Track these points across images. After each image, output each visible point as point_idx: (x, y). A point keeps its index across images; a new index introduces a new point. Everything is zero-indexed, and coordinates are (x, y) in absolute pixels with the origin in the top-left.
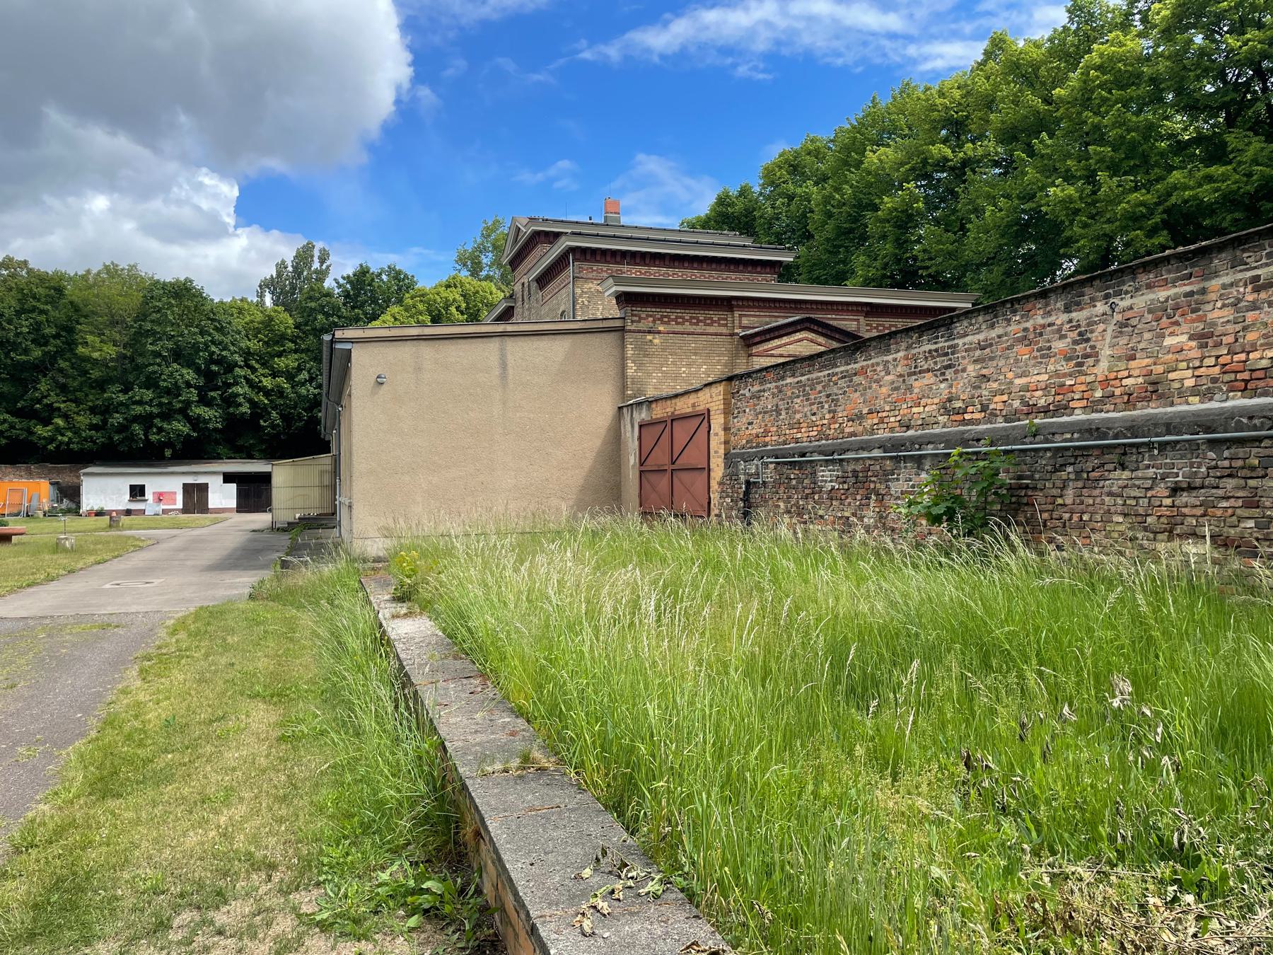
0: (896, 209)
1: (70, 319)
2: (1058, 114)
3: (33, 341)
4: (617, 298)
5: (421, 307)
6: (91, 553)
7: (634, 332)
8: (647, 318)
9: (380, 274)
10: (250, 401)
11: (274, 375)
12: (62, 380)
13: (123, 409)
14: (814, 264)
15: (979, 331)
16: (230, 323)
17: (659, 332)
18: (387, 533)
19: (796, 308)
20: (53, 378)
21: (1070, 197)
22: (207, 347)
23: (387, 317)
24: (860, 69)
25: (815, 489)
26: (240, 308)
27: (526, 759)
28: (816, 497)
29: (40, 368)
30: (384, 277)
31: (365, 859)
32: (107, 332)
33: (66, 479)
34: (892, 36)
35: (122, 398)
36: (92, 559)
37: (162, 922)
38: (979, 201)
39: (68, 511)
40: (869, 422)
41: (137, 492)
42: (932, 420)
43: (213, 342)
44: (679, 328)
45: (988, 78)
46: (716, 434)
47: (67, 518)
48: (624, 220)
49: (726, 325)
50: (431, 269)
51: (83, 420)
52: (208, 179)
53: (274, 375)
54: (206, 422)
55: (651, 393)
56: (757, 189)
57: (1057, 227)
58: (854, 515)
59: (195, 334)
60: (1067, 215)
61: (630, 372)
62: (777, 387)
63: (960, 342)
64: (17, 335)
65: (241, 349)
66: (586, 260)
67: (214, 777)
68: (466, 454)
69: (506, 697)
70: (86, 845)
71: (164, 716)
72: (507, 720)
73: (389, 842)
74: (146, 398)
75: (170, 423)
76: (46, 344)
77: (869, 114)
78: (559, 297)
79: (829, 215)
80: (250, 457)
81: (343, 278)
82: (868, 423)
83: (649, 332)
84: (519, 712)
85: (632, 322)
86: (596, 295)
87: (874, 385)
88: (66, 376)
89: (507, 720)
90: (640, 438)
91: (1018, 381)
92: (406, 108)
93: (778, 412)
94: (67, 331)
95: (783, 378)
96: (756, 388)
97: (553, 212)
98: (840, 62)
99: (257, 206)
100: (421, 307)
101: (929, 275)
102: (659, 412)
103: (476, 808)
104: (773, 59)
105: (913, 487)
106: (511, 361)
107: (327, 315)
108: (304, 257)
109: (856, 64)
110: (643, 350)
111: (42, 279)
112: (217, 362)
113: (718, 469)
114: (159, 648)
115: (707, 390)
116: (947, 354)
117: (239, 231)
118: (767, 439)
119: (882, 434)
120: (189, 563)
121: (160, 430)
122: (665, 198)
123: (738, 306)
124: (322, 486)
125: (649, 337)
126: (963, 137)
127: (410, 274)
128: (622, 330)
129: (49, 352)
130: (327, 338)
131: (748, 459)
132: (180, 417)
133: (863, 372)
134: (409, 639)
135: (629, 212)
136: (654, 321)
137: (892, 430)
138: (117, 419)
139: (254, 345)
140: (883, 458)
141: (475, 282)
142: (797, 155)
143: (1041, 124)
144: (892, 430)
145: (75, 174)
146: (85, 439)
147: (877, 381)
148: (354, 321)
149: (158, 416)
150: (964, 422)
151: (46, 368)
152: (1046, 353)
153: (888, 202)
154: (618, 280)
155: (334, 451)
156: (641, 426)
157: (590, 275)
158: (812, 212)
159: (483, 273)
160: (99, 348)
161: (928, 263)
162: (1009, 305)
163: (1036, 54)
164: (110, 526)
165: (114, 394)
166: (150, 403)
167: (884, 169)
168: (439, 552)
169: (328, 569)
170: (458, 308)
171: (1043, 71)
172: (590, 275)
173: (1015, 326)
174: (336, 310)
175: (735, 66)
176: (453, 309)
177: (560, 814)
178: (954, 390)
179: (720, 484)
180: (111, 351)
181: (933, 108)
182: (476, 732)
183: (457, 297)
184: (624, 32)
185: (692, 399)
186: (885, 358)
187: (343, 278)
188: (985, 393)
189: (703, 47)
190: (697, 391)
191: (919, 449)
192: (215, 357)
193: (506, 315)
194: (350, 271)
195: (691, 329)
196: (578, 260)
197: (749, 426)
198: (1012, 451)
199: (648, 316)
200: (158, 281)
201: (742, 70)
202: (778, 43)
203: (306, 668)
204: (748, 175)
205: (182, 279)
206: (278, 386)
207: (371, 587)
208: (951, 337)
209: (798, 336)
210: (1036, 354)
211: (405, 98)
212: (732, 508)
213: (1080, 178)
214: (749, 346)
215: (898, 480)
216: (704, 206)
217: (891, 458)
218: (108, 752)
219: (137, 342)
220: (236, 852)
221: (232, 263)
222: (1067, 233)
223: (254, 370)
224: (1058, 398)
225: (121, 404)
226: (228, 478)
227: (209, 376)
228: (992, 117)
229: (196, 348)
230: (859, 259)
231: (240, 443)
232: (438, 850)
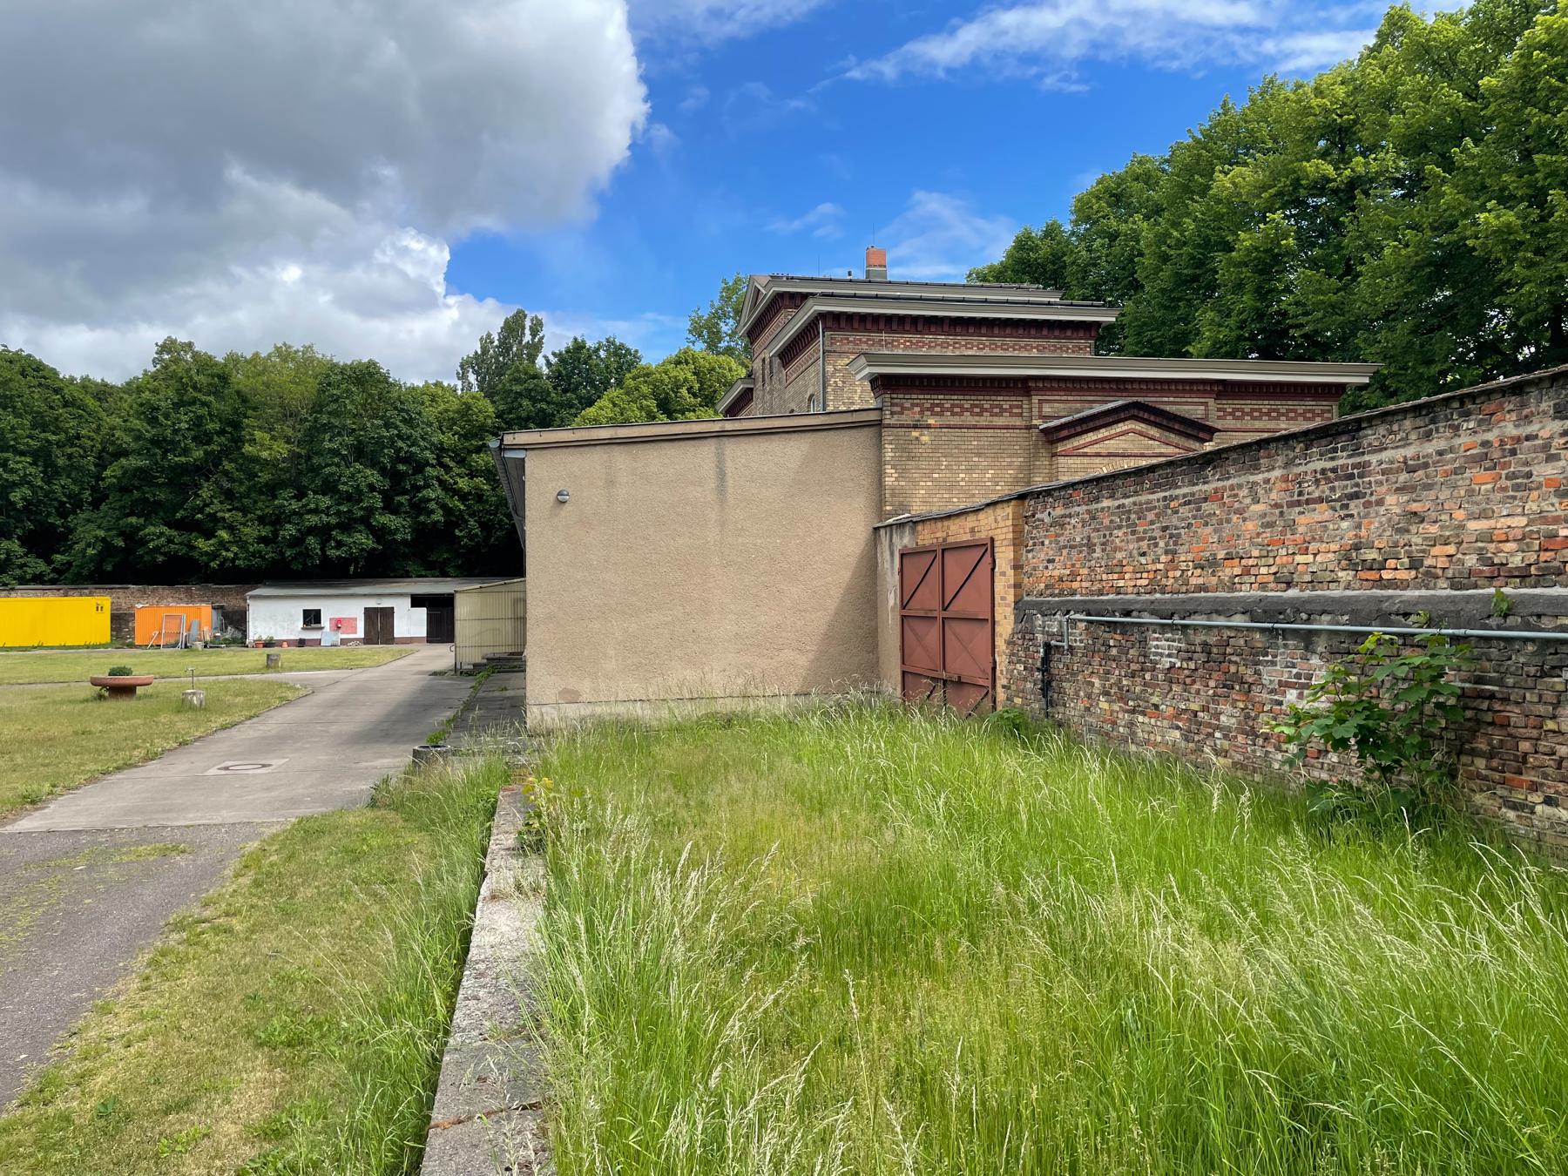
0: (1256, 249)
1: (235, 411)
2: (1488, 112)
3: (194, 439)
4: (872, 382)
5: (645, 389)
8: (912, 407)
9: (597, 350)
10: (444, 507)
11: (472, 475)
13: (295, 519)
14: (1145, 324)
15: (1405, 442)
16: (419, 414)
17: (929, 427)
19: (1119, 390)
21: (1508, 225)
24: (1201, 74)
25: (1146, 664)
26: (434, 394)
28: (1148, 676)
29: (202, 470)
30: (602, 354)
33: (231, 602)
34: (1243, 30)
35: (295, 505)
36: (221, 720)
38: (1372, 234)
40: (1228, 571)
41: (312, 618)
42: (1328, 576)
43: (400, 436)
44: (956, 421)
45: (1384, 68)
46: (1003, 574)
48: (894, 274)
49: (1021, 415)
50: (656, 340)
51: (250, 532)
52: (415, 244)
53: (472, 475)
55: (918, 509)
56: (1068, 227)
57: (1487, 265)
58: (1205, 709)
59: (378, 427)
60: (1505, 250)
61: (889, 481)
62: (1089, 512)
63: (1373, 459)
64: (176, 432)
66: (840, 329)
68: (686, 581)
74: (323, 506)
75: (350, 536)
76: (208, 443)
77: (1219, 123)
78: (807, 375)
79: (1165, 258)
80: (445, 574)
82: (1226, 572)
83: (915, 427)
85: (892, 413)
87: (1235, 518)
88: (232, 480)
90: (901, 571)
91: (1473, 525)
93: (1091, 547)
94: (233, 426)
95: (1097, 500)
96: (1059, 511)
97: (802, 268)
98: (1175, 65)
99: (471, 270)
100: (645, 389)
101: (1305, 336)
102: (928, 537)
104: (1089, 66)
105: (1302, 687)
106: (730, 466)
107: (534, 401)
108: (513, 328)
109: (1196, 67)
111: (204, 363)
112: (404, 461)
113: (1006, 624)
115: (990, 511)
116: (1351, 477)
117: (451, 300)
118: (1075, 585)
119: (1247, 592)
121: (339, 544)
122: (946, 245)
123: (1038, 389)
125: (915, 434)
126: (1349, 149)
127: (633, 348)
128: (878, 424)
129: (212, 451)
131: (1048, 611)
132: (362, 528)
133: (1216, 496)
135: (899, 262)
136: (922, 412)
137: (1263, 586)
138: (289, 530)
139: (448, 439)
140: (1248, 629)
141: (711, 357)
142: (1121, 180)
143: (1463, 127)
144: (1263, 586)
145: (266, 237)
146: (253, 554)
147: (1240, 512)
149: (338, 526)
150: (1380, 583)
151: (210, 472)
152: (1523, 483)
153: (1246, 240)
154: (872, 359)
156: (902, 556)
157: (845, 348)
158: (1141, 254)
159: (723, 345)
160: (269, 446)
161: (1303, 320)
162: (1456, 405)
163: (1452, 32)
164: (268, 666)
167: (1239, 195)
170: (689, 390)
171: (1462, 56)
173: (1468, 437)
174: (544, 396)
175: (1040, 77)
176: (684, 391)
178: (1363, 532)
180: (282, 449)
181: (1307, 111)
185: (970, 521)
186: (1252, 478)
188: (1415, 540)
189: (998, 56)
190: (977, 511)
191: (1308, 621)
192: (402, 454)
194: (562, 347)
195: (972, 420)
196: (830, 329)
197: (1050, 564)
198: (1466, 637)
200: (336, 365)
201: (1050, 82)
202: (1095, 46)
204: (1056, 207)
208: (1357, 451)
209: (1121, 427)
210: (1504, 483)
212: (1025, 679)
213: (1522, 199)
214: (1053, 442)
215: (1273, 663)
216: (998, 253)
217: (1263, 630)
221: (424, 335)
222: (1504, 276)
223: (448, 469)
224: (1545, 556)
225: (294, 513)
226: (417, 601)
227: (395, 477)
228: (1392, 119)
230: (1205, 316)
231: (433, 558)
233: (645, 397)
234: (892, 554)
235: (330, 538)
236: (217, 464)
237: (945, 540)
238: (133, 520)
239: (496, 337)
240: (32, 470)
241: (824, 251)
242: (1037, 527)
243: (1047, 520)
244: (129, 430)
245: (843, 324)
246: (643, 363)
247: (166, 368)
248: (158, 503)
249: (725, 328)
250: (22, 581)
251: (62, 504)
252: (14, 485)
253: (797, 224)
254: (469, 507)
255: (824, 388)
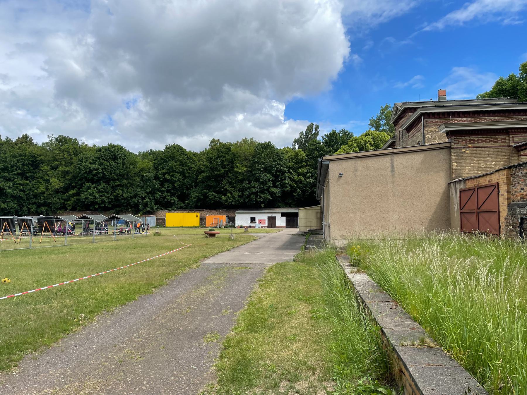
5: (355, 145)
6: (240, 241)
7: (456, 148)
8: (462, 141)
10: (290, 185)
12: (230, 180)
17: (469, 147)
18: (343, 237)
20: (227, 180)
22: (276, 166)
23: (341, 150)
26: (286, 151)
27: (422, 341)
29: (224, 176)
31: (351, 373)
32: (243, 163)
35: (248, 186)
36: (240, 243)
37: (276, 384)
39: (231, 226)
44: (480, 145)
46: (503, 195)
47: (232, 228)
48: (448, 98)
49: (505, 142)
50: (359, 128)
51: (236, 194)
52: (275, 104)
54: (275, 194)
55: (465, 176)
56: (518, 76)
64: (217, 165)
65: (287, 166)
66: (429, 118)
67: (289, 330)
68: (383, 206)
69: (407, 312)
70: (248, 349)
71: (269, 304)
72: (410, 322)
73: (360, 368)
74: (256, 186)
78: (417, 135)
80: (290, 207)
81: (325, 135)
83: (464, 148)
84: (415, 320)
85: (455, 144)
86: (436, 133)
88: (231, 179)
89: (410, 322)
90: (460, 197)
92: (348, 66)
94: (232, 162)
99: (292, 112)
100: (355, 145)
102: (470, 185)
103: (402, 360)
107: (318, 151)
108: (310, 129)
110: (461, 157)
111: (224, 145)
112: (279, 171)
113: (504, 212)
114: (265, 277)
120: (271, 246)
121: (260, 197)
122: (469, 84)
124: (317, 218)
125: (464, 150)
127: (351, 132)
128: (450, 148)
130: (320, 160)
134: (359, 283)
135: (450, 94)
136: (466, 143)
138: (247, 193)
139: (292, 164)
148: (327, 153)
149: (260, 192)
154: (447, 126)
155: (321, 204)
156: (460, 192)
157: (432, 125)
159: (381, 128)
160: (241, 168)
165: (246, 185)
166: (257, 187)
168: (372, 247)
169: (323, 251)
170: (370, 144)
172: (432, 125)
174: (322, 149)
175: (502, 20)
176: (368, 145)
177: (443, 368)
179: (505, 219)
180: (245, 169)
182: (396, 326)
183: (370, 139)
184: (445, 15)
185: (488, 178)
187: (325, 135)
189: (485, 15)
190: (491, 174)
193: (392, 145)
195: (486, 145)
196: (426, 118)
199: (463, 140)
200: (259, 143)
201: (506, 22)
203: (317, 291)
205: (267, 142)
206: (300, 179)
207: (341, 260)
211: (347, 61)
216: (489, 86)
218: (252, 315)
219: (253, 165)
220: (300, 361)
221: (284, 134)
223: (291, 174)
225: (248, 188)
226: (283, 215)
227: (276, 176)
229: (272, 166)
232: (382, 375)
233: (355, 147)
234: (456, 192)
235: (258, 195)
236: (227, 173)
237: (478, 185)
238: (205, 191)
239: (304, 132)
240: (180, 177)
241: (420, 92)
242: (516, 178)
243: (520, 175)
244: (204, 165)
245: (431, 116)
246: (354, 136)
247: (212, 147)
248: (212, 186)
249: (382, 123)
250: (178, 208)
251: (187, 186)
252: (176, 181)
253: (406, 84)
254: (298, 185)
255: (424, 139)
